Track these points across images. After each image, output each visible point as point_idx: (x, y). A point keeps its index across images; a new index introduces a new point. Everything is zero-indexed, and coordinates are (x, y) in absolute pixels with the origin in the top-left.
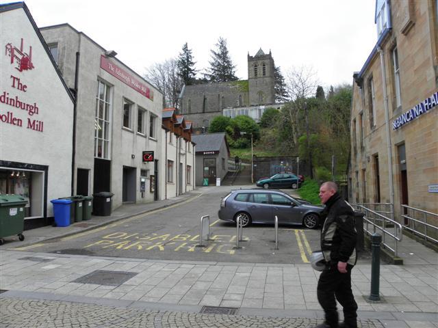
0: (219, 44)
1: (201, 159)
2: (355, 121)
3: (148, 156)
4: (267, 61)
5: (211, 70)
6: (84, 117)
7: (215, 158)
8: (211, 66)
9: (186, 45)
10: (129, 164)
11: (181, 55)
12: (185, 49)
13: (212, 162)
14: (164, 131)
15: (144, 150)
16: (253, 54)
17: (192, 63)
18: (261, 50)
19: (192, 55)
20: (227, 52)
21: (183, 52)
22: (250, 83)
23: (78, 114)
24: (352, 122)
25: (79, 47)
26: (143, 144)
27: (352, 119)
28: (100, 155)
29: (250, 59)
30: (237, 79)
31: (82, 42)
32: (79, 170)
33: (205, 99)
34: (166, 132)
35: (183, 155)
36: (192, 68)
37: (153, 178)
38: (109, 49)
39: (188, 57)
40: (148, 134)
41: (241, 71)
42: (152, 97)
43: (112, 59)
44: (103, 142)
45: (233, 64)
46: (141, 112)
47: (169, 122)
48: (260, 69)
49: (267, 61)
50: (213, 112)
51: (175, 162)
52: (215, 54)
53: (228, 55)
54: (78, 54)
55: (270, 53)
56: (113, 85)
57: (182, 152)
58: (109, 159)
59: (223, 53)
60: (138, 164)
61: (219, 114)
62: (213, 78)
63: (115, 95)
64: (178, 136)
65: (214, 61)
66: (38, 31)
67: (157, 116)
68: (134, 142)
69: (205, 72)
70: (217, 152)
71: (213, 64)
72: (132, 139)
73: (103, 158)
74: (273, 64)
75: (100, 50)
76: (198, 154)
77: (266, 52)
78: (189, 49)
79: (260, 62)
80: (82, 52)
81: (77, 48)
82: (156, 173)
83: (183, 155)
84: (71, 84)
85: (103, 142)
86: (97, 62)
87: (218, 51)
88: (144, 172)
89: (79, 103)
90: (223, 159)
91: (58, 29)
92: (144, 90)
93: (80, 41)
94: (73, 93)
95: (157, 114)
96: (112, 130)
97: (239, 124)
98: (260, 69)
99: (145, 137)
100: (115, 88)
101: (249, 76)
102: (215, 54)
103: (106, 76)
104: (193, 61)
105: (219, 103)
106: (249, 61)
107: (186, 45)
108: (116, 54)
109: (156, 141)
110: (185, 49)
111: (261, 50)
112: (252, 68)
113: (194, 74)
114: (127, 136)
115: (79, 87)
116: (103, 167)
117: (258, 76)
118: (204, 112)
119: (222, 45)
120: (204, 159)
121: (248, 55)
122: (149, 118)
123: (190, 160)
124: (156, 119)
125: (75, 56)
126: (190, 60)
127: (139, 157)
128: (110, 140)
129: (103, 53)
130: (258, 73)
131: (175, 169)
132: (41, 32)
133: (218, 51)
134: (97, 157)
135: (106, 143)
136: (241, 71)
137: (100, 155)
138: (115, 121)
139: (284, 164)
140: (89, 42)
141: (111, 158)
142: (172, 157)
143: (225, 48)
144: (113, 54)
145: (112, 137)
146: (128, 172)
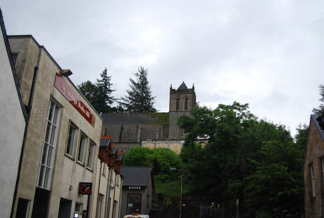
0: (139, 73)
1: (126, 193)
2: (311, 165)
3: (85, 188)
4: (189, 96)
5: (128, 99)
6: (33, 139)
7: (141, 195)
8: (128, 96)
9: (105, 72)
10: (65, 196)
11: (99, 81)
12: (104, 74)
13: (137, 198)
14: (99, 161)
15: (81, 182)
16: (176, 87)
17: (110, 91)
18: (183, 85)
19: (111, 82)
20: (147, 83)
21: (101, 79)
22: (171, 117)
23: (29, 135)
24: (306, 166)
25: (38, 61)
26: (81, 175)
27: (307, 162)
28: (40, 184)
29: (172, 91)
30: (155, 110)
31: (42, 56)
32: (20, 200)
33: (122, 128)
34: (101, 162)
35: (113, 188)
36: (110, 95)
37: (85, 213)
38: (64, 67)
39: (106, 84)
40: (76, 158)
41: (162, 105)
42: (94, 123)
43: (65, 78)
44: (45, 169)
45: (152, 95)
46: (83, 136)
47: (104, 151)
48: (182, 102)
49: (189, 96)
50: (130, 143)
51: (118, 202)
52: (134, 83)
53: (148, 85)
54: (36, 69)
55: (193, 88)
56: (62, 107)
57: (112, 185)
58: (48, 188)
59: (142, 82)
60: (74, 197)
61: (135, 146)
62: (130, 107)
63: (63, 117)
64: (110, 167)
65: (132, 91)
66: (7, 38)
67: (96, 144)
68: (73, 171)
69: (122, 101)
70: (143, 188)
71: (131, 94)
72: (72, 168)
73: (42, 187)
74: (195, 99)
75: (56, 67)
76: (124, 188)
77: (189, 87)
78: (108, 75)
79: (182, 96)
80: (40, 66)
81: (36, 62)
82: (88, 208)
83: (113, 188)
84: (27, 104)
85: (45, 169)
86: (51, 79)
87: (137, 80)
88: (78, 205)
89: (31, 122)
90: (148, 196)
91: (20, 40)
92: (88, 115)
93: (40, 55)
94: (27, 110)
95: (96, 142)
96: (56, 157)
97: (160, 159)
98: (182, 102)
99: (73, 160)
100: (64, 110)
101: (170, 109)
102: (134, 83)
103: (58, 97)
104: (112, 88)
105: (137, 131)
106: (171, 93)
107: (105, 72)
108: (71, 73)
109: (92, 171)
110: (104, 74)
111: (183, 85)
112: (174, 101)
113: (111, 102)
114: (68, 163)
115: (33, 105)
116: (43, 196)
117: (180, 110)
118: (120, 143)
119: (143, 75)
120: (128, 194)
121: (171, 88)
122: (88, 146)
123: (117, 194)
124: (94, 147)
125: (33, 71)
126: (108, 87)
127: (76, 187)
128: (51, 167)
129: (58, 71)
130: (180, 107)
131: (118, 208)
132: (9, 40)
133: (137, 80)
134: (37, 186)
135: (48, 169)
136: (162, 105)
137: (40, 184)
138: (59, 146)
139: (216, 205)
140: (48, 57)
141: (51, 187)
142: (103, 191)
143: (145, 79)
144: (69, 73)
145: (55, 164)
146: (65, 204)
